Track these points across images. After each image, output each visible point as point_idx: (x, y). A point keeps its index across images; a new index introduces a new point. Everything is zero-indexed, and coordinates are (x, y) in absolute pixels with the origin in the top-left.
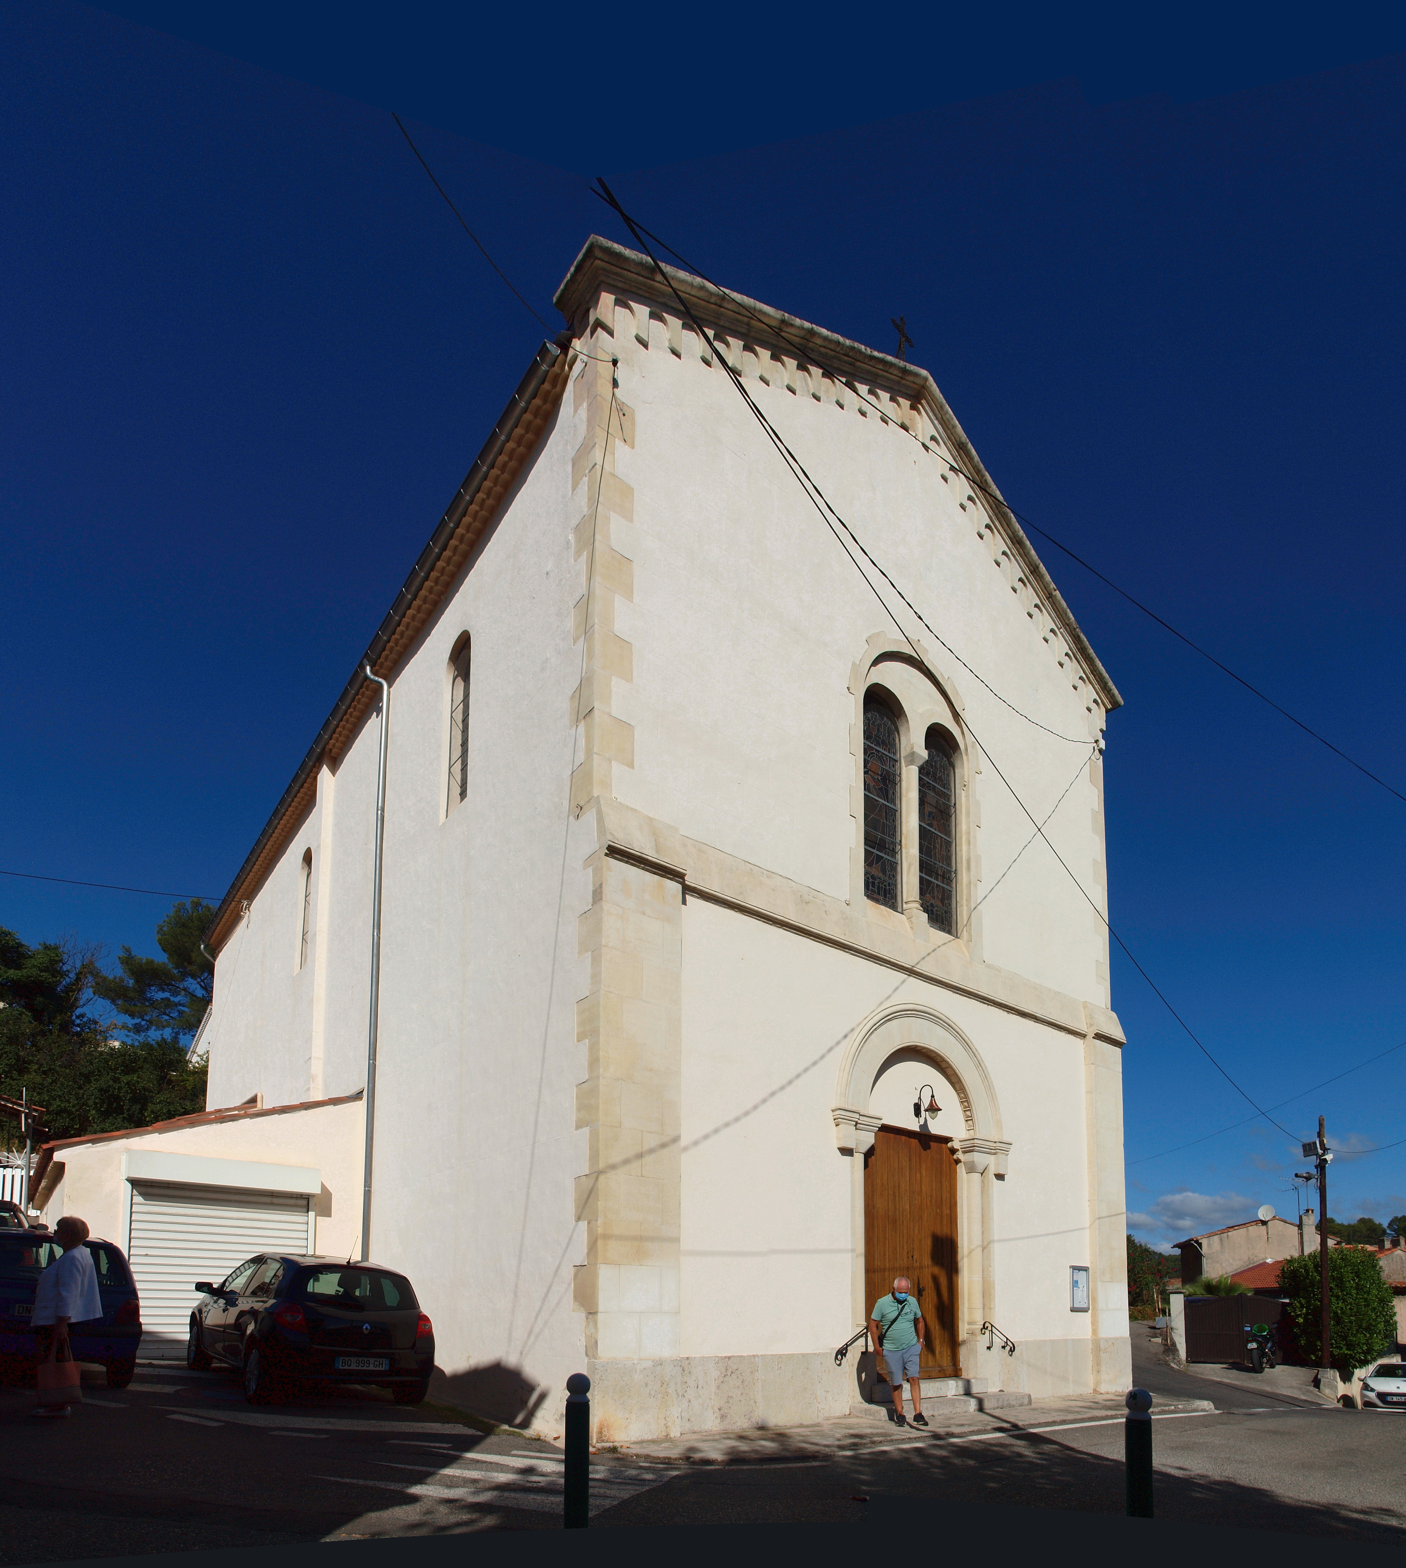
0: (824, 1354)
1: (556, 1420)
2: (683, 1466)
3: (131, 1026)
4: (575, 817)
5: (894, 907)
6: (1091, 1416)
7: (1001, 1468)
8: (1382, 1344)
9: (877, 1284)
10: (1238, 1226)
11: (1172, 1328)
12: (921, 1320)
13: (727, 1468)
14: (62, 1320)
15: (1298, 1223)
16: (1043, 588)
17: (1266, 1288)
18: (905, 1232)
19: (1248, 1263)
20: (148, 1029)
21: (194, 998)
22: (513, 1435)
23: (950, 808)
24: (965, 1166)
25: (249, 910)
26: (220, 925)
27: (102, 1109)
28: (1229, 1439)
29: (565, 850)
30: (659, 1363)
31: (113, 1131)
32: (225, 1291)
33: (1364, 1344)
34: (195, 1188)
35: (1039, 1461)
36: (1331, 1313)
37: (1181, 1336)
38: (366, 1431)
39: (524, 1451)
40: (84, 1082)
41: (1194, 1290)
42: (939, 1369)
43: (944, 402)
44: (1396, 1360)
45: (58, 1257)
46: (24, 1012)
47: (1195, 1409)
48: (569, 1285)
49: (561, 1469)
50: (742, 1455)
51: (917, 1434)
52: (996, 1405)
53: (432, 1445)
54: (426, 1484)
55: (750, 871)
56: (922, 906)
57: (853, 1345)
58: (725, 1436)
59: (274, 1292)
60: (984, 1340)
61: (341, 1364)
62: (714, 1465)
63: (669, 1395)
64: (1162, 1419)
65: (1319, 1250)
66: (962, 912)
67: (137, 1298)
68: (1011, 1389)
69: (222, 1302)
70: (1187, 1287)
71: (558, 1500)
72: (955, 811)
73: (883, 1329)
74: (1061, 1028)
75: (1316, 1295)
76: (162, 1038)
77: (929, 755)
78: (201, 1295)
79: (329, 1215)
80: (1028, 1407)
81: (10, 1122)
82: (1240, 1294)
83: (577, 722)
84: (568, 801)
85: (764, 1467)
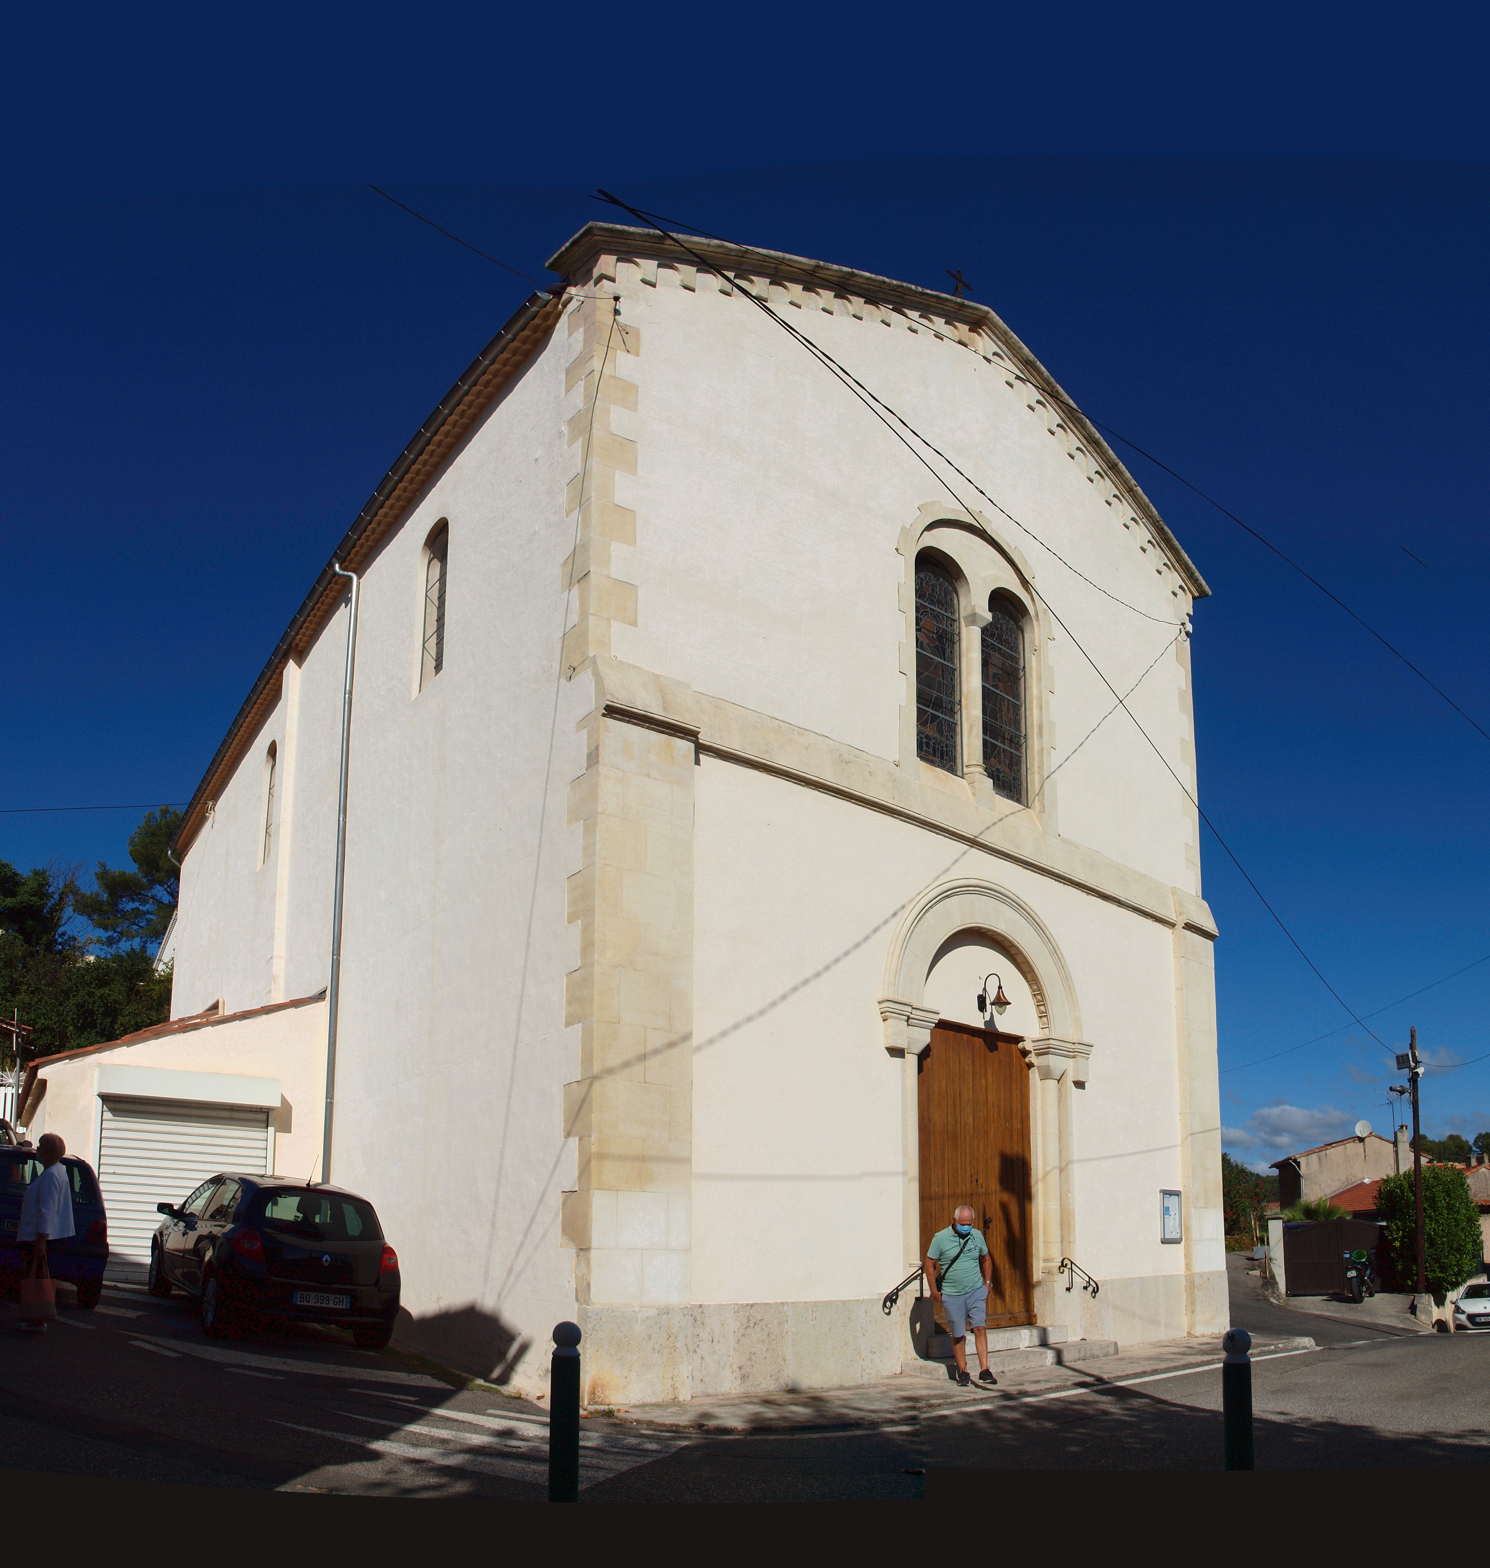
0: (869, 1301)
1: (540, 1375)
2: (694, 1436)
3: (104, 939)
4: (566, 678)
5: (952, 770)
6: (1185, 1363)
7: (1084, 1428)
8: (1471, 1265)
9: (933, 1214)
10: (1336, 1143)
11: (1270, 1259)
12: (988, 1257)
13: (749, 1437)
14: (42, 1236)
15: (1393, 1141)
16: (1123, 482)
17: (1364, 1210)
18: (968, 1150)
19: (1346, 1183)
20: (119, 941)
21: (161, 905)
22: (490, 1391)
23: (1019, 672)
24: (1038, 1071)
25: (214, 810)
26: (186, 829)
27: (79, 1025)
28: (1330, 1377)
29: (555, 714)
30: (665, 1311)
31: (88, 1046)
32: (185, 1213)
33: (1455, 1265)
34: (162, 1103)
35: (1127, 1419)
36: (1425, 1235)
37: (1280, 1267)
38: (325, 1376)
39: (501, 1410)
40: (64, 999)
41: (1293, 1215)
42: (1009, 1316)
43: (1009, 330)
44: (1482, 1280)
45: (39, 1174)
46: (17, 937)
47: (1295, 1348)
48: (557, 1215)
49: (546, 1434)
50: (768, 1422)
51: (983, 1394)
52: (1077, 1356)
53: (396, 1396)
54: (389, 1440)
55: (778, 728)
56: (986, 771)
57: (905, 1289)
58: (746, 1400)
59: (232, 1216)
60: (1062, 1280)
61: (300, 1299)
62: (733, 1435)
63: (677, 1350)
64: (1261, 1361)
65: (1413, 1168)
66: (1033, 780)
67: (105, 1218)
68: (1094, 1337)
69: (182, 1224)
70: (1286, 1211)
71: (542, 1468)
72: (1024, 675)
73: (942, 1269)
74: (1148, 915)
75: (1411, 1216)
76: (132, 948)
77: (994, 617)
78: (163, 1217)
79: (289, 1131)
80: (1114, 1357)
81: (5, 1043)
82: (1339, 1218)
83: (570, 586)
84: (559, 663)
85: (795, 1437)
